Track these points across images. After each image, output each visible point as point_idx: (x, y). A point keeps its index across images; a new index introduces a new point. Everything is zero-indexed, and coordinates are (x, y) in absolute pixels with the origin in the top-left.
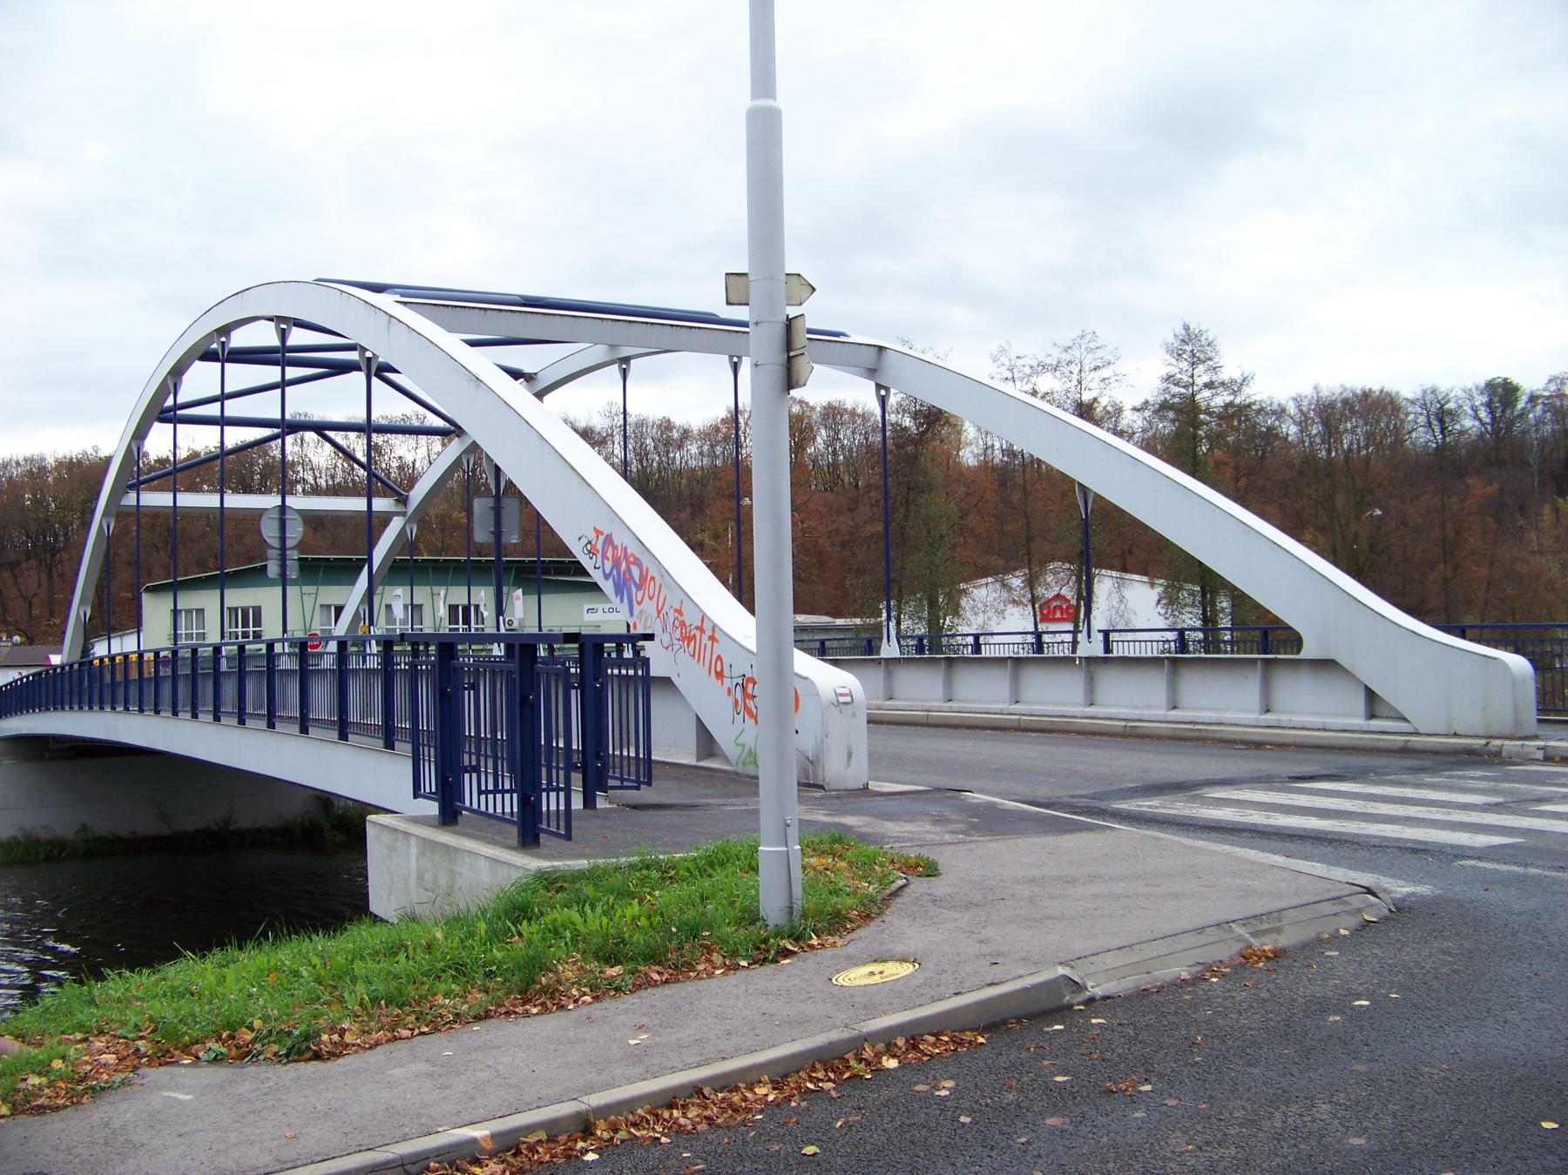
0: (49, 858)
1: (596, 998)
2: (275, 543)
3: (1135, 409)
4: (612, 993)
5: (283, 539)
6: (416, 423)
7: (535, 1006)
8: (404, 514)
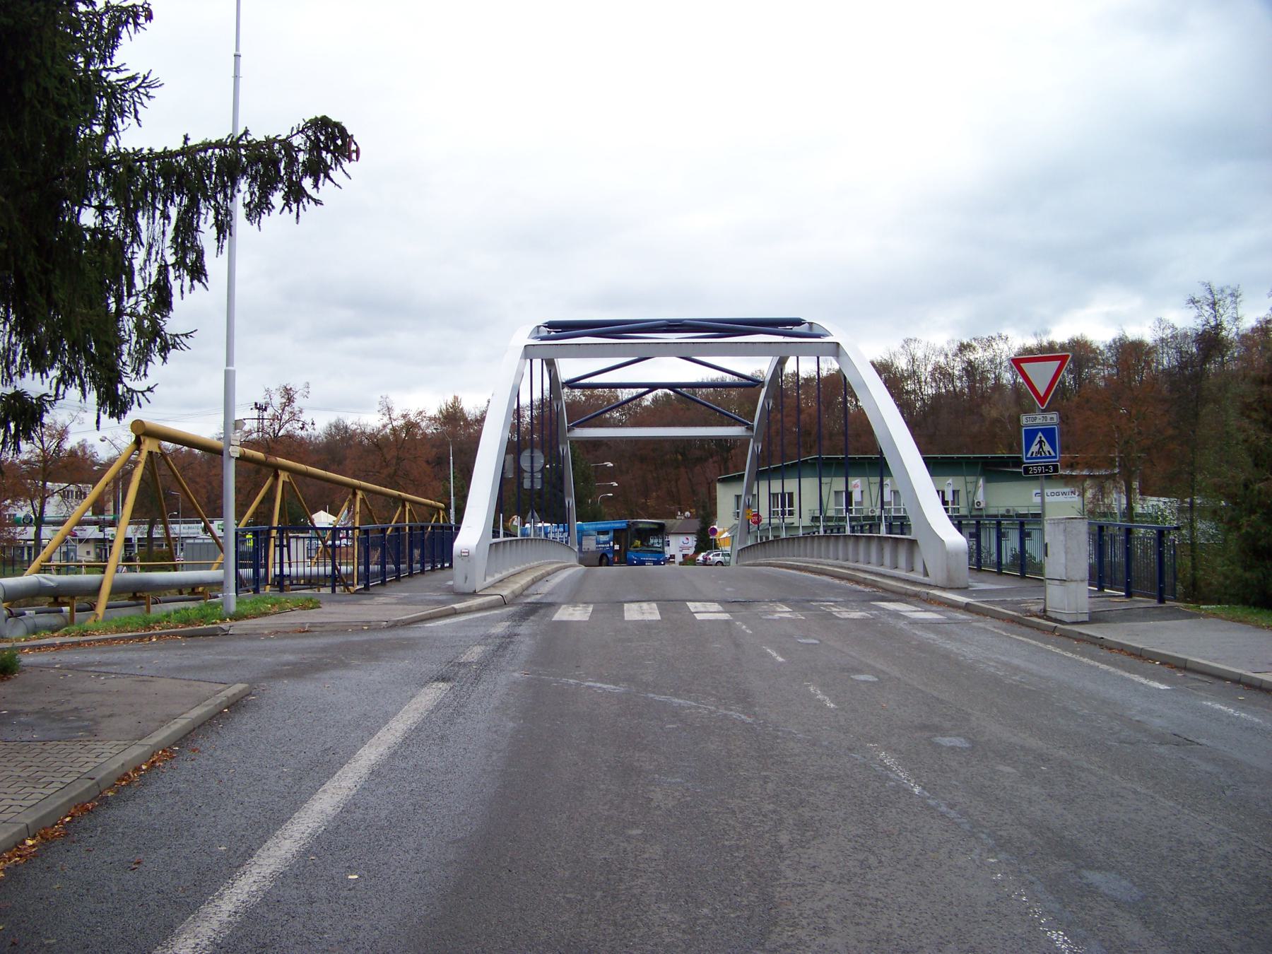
2: (529, 469)
5: (532, 467)
6: (630, 396)
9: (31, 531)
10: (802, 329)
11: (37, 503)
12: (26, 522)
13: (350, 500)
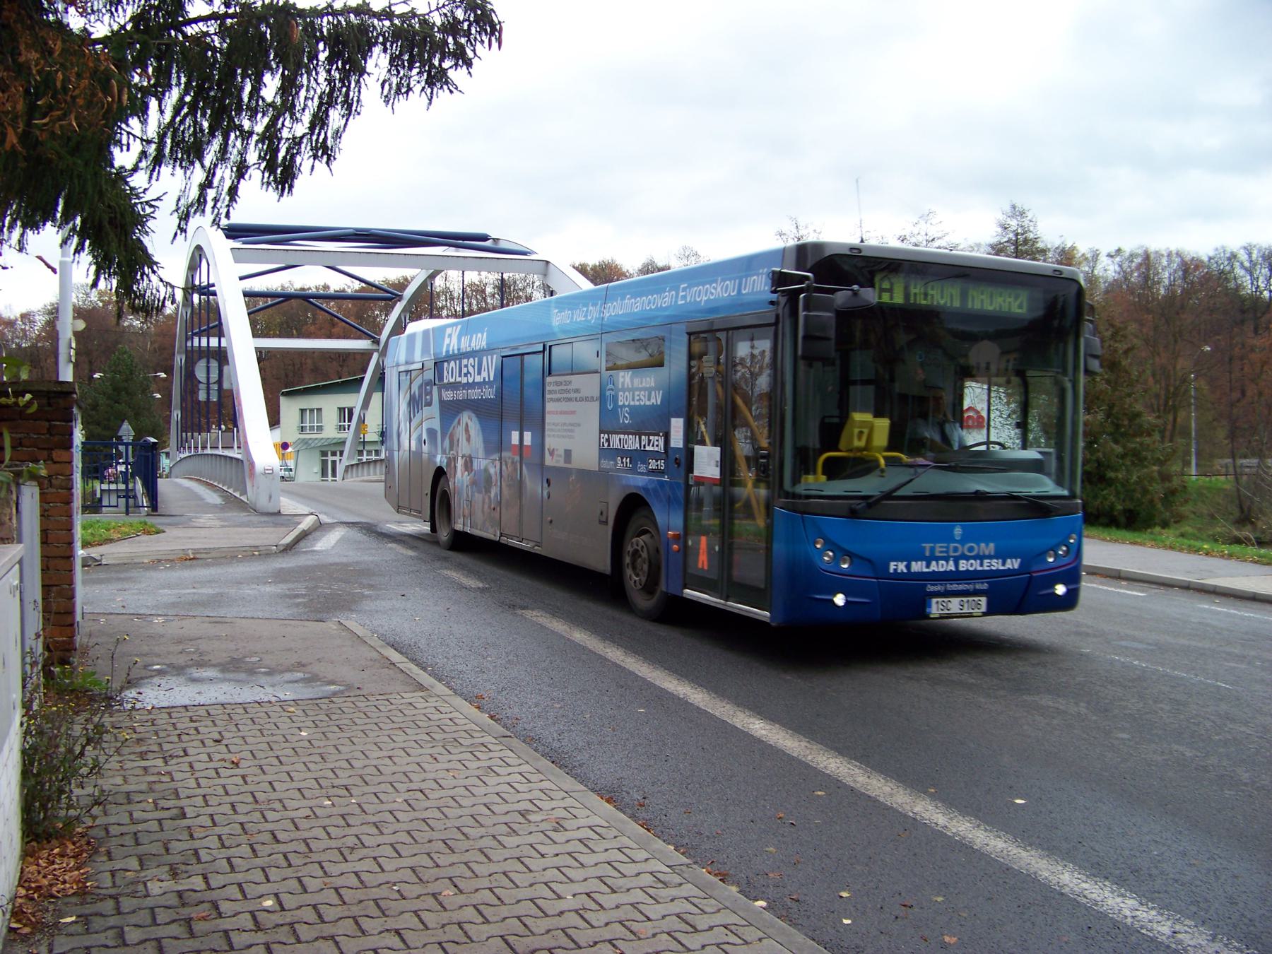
3: (1110, 256)
5: (208, 378)
8: (377, 351)
10: (488, 244)
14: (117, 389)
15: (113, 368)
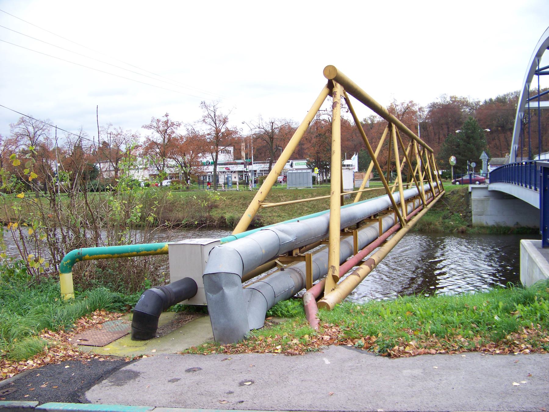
0: (504, 233)
1: (532, 351)
4: (542, 350)
7: (500, 349)
9: (211, 168)
11: (214, 154)
12: (208, 164)
13: (411, 146)
14: (468, 137)
15: (466, 127)
